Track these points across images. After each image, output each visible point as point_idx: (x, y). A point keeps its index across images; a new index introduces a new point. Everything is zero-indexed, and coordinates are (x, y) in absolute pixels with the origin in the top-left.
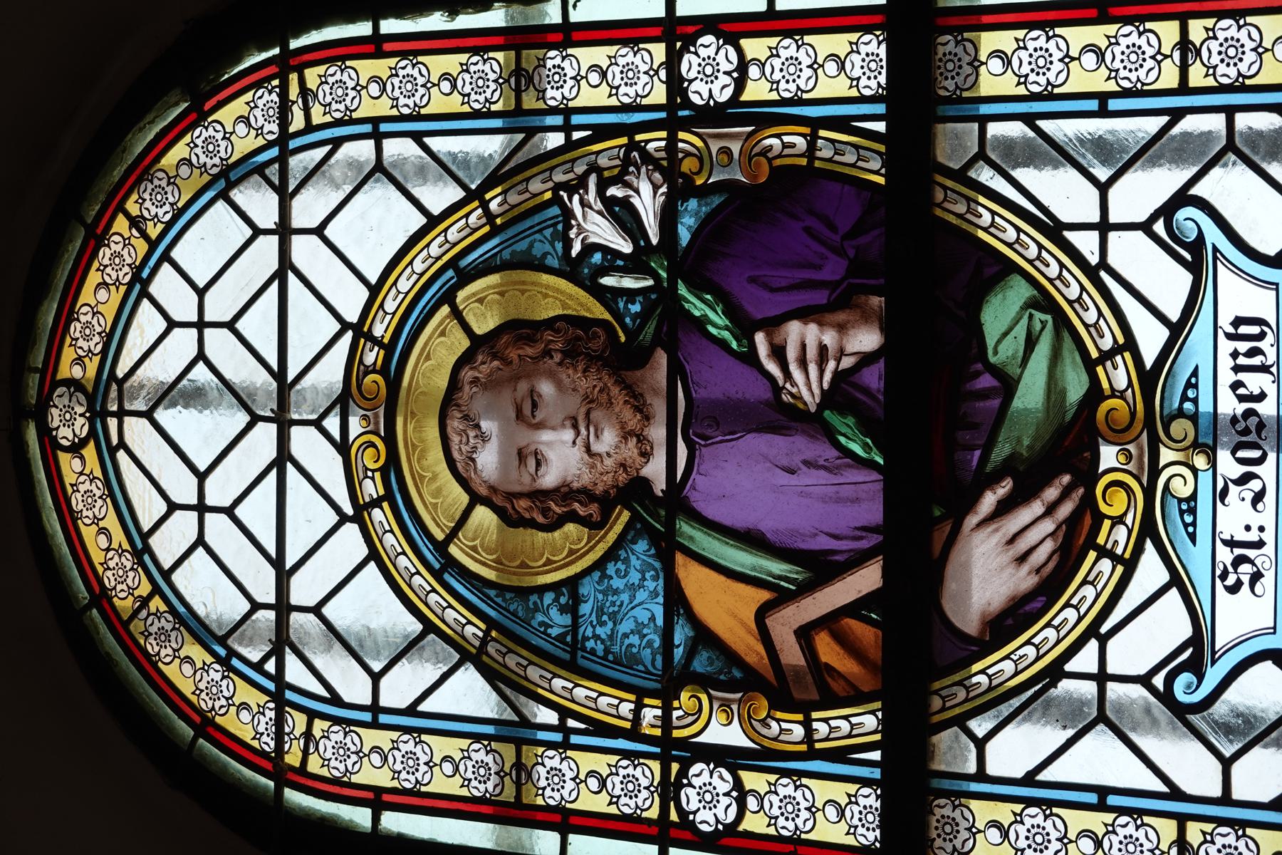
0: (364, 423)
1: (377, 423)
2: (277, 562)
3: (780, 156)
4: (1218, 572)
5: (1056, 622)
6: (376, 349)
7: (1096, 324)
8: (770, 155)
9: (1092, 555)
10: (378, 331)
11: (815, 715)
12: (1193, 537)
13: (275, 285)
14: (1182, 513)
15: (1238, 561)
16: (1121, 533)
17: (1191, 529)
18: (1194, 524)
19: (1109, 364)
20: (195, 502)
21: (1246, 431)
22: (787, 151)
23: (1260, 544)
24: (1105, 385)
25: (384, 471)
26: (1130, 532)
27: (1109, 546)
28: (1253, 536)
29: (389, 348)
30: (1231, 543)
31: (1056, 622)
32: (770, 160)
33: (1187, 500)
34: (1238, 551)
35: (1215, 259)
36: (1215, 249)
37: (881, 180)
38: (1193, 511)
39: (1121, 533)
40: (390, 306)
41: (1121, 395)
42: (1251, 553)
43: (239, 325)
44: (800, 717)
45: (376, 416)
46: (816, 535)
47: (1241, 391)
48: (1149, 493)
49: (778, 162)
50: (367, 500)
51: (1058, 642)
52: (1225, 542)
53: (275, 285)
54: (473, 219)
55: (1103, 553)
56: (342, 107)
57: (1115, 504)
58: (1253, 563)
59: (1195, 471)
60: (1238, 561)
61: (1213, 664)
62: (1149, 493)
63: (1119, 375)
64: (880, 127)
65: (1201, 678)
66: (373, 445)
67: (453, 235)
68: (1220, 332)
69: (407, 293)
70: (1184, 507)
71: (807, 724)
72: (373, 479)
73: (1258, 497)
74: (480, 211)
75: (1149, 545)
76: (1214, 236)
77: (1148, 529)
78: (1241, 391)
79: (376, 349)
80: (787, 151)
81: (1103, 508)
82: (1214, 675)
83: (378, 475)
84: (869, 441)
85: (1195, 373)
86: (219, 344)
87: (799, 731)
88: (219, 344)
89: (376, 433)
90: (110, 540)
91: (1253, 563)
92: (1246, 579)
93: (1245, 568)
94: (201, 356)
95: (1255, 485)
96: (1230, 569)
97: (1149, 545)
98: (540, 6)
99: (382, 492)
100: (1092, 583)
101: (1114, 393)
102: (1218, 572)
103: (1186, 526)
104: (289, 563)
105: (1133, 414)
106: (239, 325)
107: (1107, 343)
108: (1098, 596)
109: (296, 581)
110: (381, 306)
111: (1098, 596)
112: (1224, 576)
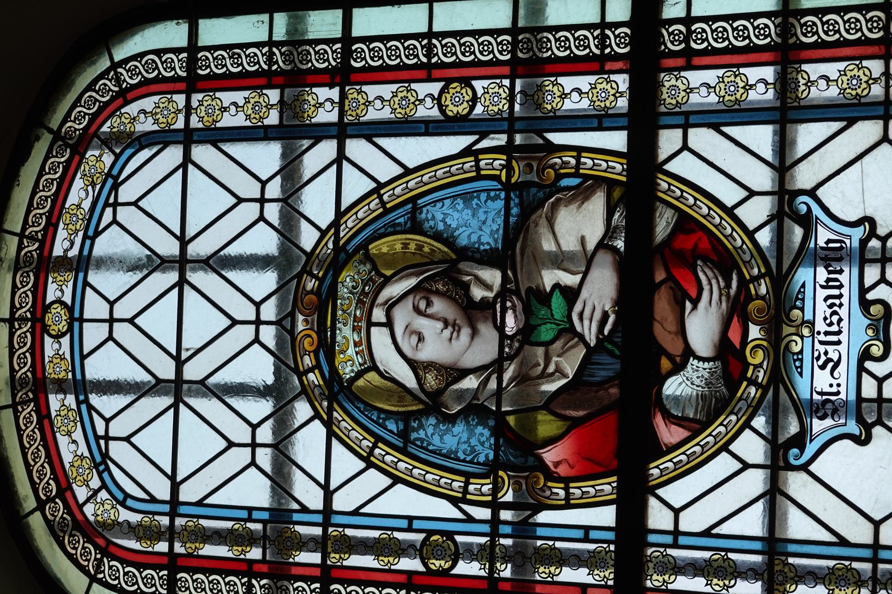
0: (304, 323)
1: (313, 324)
2: (172, 477)
4: (814, 409)
6: (314, 280)
11: (571, 485)
12: (801, 374)
14: (795, 361)
17: (799, 370)
18: (801, 367)
20: (254, 326)
21: (831, 324)
23: (839, 343)
24: (753, 292)
25: (316, 353)
27: (754, 377)
28: (834, 389)
32: (555, 171)
33: (798, 354)
34: (824, 397)
35: (817, 222)
36: (817, 218)
37: (624, 179)
38: (801, 360)
44: (562, 485)
45: (313, 321)
47: (830, 268)
50: (306, 368)
51: (727, 433)
52: (818, 393)
56: (354, 114)
59: (802, 337)
61: (810, 442)
65: (802, 451)
68: (817, 285)
70: (795, 357)
71: (566, 489)
72: (309, 355)
74: (377, 200)
76: (817, 211)
78: (830, 268)
79: (314, 280)
81: (750, 360)
82: (811, 449)
83: (312, 354)
84: (612, 319)
85: (803, 286)
87: (562, 493)
89: (312, 329)
98: (528, 25)
99: (314, 363)
102: (814, 409)
103: (797, 368)
104: (179, 479)
109: (183, 488)
112: (818, 358)
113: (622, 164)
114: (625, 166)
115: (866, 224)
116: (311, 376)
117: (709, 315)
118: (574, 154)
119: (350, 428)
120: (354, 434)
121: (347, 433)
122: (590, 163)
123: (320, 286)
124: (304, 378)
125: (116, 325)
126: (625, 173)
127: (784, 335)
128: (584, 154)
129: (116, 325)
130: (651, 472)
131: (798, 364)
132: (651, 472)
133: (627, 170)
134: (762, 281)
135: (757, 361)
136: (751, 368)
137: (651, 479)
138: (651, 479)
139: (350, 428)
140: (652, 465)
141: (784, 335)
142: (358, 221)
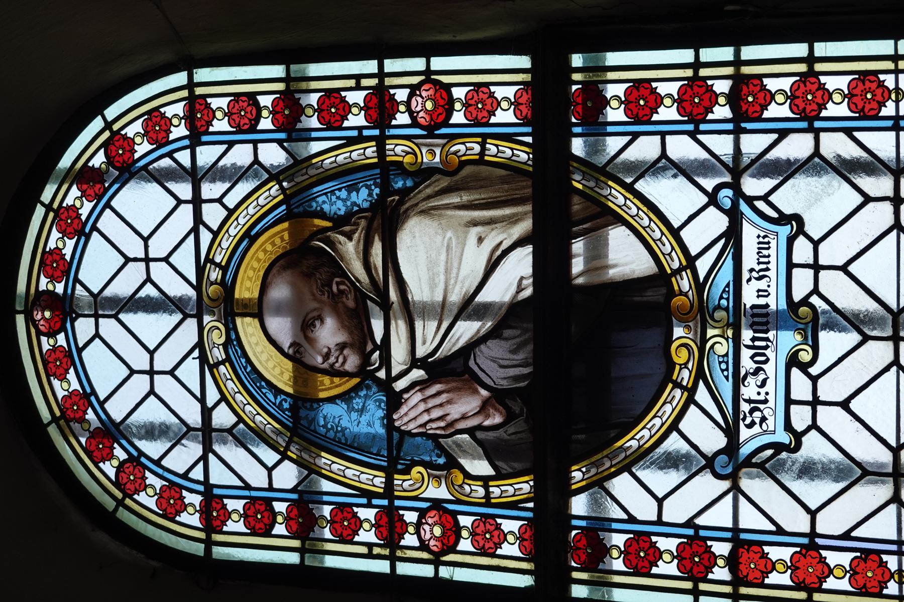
3: (464, 155)
5: (649, 426)
7: (669, 255)
8: (460, 154)
9: (670, 386)
10: (218, 259)
13: (192, 236)
14: (720, 363)
15: (752, 411)
16: (685, 374)
19: (678, 277)
22: (468, 152)
23: (765, 401)
24: (676, 288)
25: (225, 345)
26: (691, 372)
27: (679, 380)
28: (762, 397)
29: (224, 269)
30: (749, 401)
31: (649, 426)
33: (723, 356)
34: (752, 405)
37: (531, 169)
39: (685, 374)
40: (225, 245)
41: (686, 294)
42: (761, 406)
43: (171, 260)
46: (359, 422)
48: (701, 350)
49: (464, 158)
51: (651, 437)
52: (745, 400)
53: (192, 236)
54: (273, 191)
55: (677, 385)
57: (681, 357)
58: (762, 412)
60: (752, 411)
62: (701, 350)
63: (685, 283)
64: (529, 139)
66: (218, 328)
67: (261, 201)
69: (235, 236)
73: (763, 384)
75: (701, 383)
77: (700, 374)
80: (468, 152)
81: (676, 359)
83: (221, 347)
86: (159, 271)
88: (159, 271)
90: (70, 385)
91: (762, 412)
92: (757, 421)
93: (757, 414)
94: (149, 279)
95: (761, 377)
96: (748, 415)
97: (701, 383)
99: (224, 357)
100: (670, 402)
101: (681, 293)
103: (723, 371)
105: (692, 305)
106: (171, 260)
107: (676, 265)
108: (663, 425)
110: (219, 244)
111: (663, 425)
112: (744, 419)
113: (528, 153)
114: (531, 156)
115: (794, 223)
116: (222, 368)
117: (447, 412)
118: (479, 140)
119: (330, 463)
120: (349, 473)
121: (357, 479)
122: (494, 150)
123: (224, 276)
124: (215, 370)
125: (147, 367)
126: (530, 163)
127: (708, 337)
128: (489, 141)
129: (147, 367)
130: (573, 474)
131: (724, 366)
132: (573, 474)
133: (533, 160)
134: (684, 273)
135: (681, 361)
136: (678, 367)
137: (573, 481)
138: (573, 481)
139: (330, 463)
140: (574, 468)
141: (708, 337)
142: (259, 208)
